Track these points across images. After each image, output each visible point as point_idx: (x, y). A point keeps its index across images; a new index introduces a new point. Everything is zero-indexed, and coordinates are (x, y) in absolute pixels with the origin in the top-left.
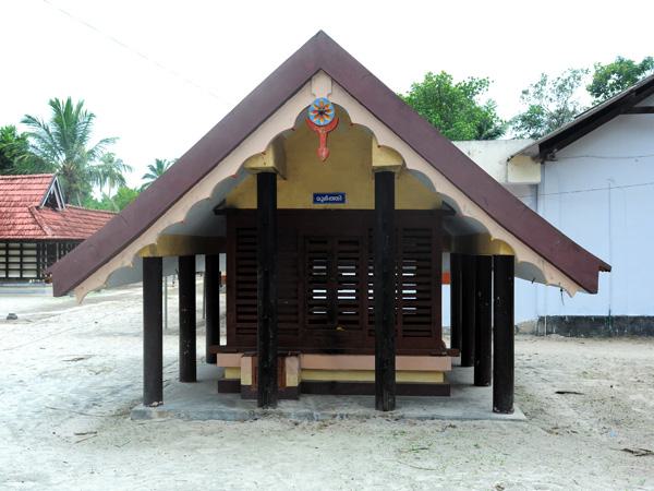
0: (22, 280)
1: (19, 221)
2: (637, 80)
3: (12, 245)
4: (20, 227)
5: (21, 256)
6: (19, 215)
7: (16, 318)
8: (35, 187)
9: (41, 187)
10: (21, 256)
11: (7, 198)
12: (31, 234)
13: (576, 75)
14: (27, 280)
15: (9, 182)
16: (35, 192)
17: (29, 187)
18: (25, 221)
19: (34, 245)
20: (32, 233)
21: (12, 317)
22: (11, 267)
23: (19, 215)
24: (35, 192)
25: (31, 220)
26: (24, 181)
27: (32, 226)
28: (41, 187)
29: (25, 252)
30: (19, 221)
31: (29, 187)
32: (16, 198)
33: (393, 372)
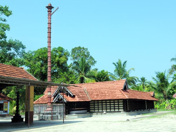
0: (115, 112)
1: (117, 94)
2: (25, 90)
3: (107, 101)
4: (118, 96)
5: (118, 104)
6: (117, 92)
7: (129, 121)
8: (121, 83)
9: (122, 83)
10: (118, 104)
11: (113, 87)
12: (121, 98)
13: (105, 114)
14: (120, 112)
15: (113, 83)
16: (121, 85)
17: (119, 84)
18: (119, 94)
19: (122, 101)
20: (122, 97)
21: (128, 120)
22: (107, 108)
23: (117, 92)
24: (121, 85)
25: (121, 93)
26: (117, 82)
27: (121, 95)
28: (122, 83)
29: (120, 103)
30: (117, 94)
31: (119, 84)
32: (116, 87)
33: (33, 117)
